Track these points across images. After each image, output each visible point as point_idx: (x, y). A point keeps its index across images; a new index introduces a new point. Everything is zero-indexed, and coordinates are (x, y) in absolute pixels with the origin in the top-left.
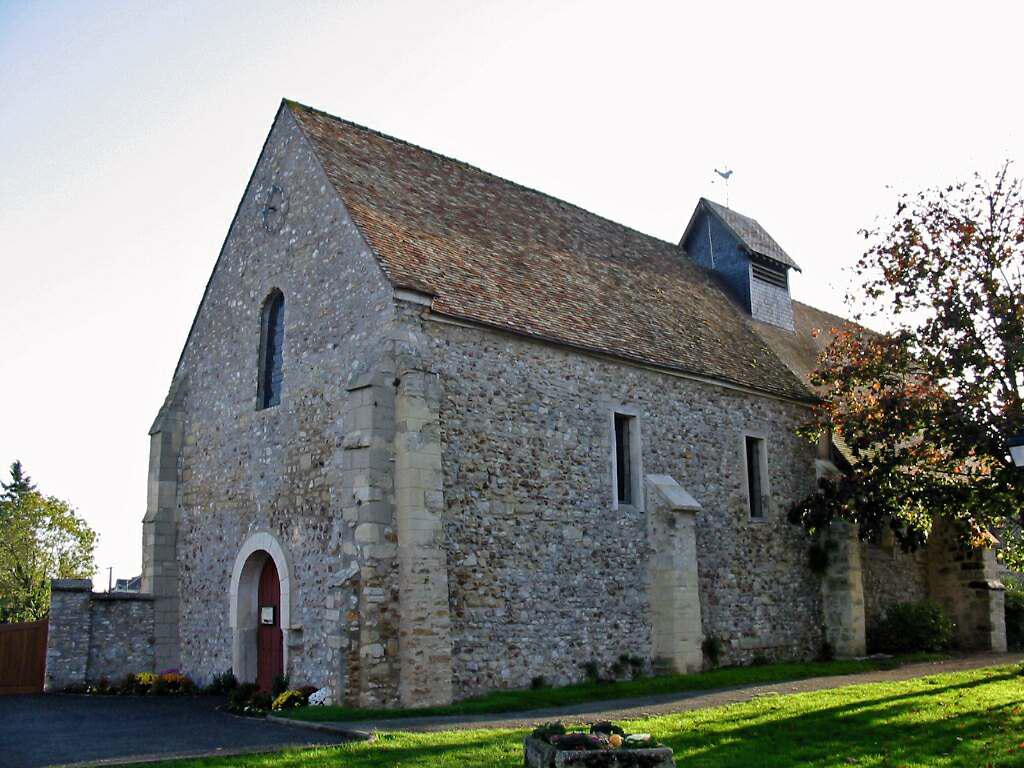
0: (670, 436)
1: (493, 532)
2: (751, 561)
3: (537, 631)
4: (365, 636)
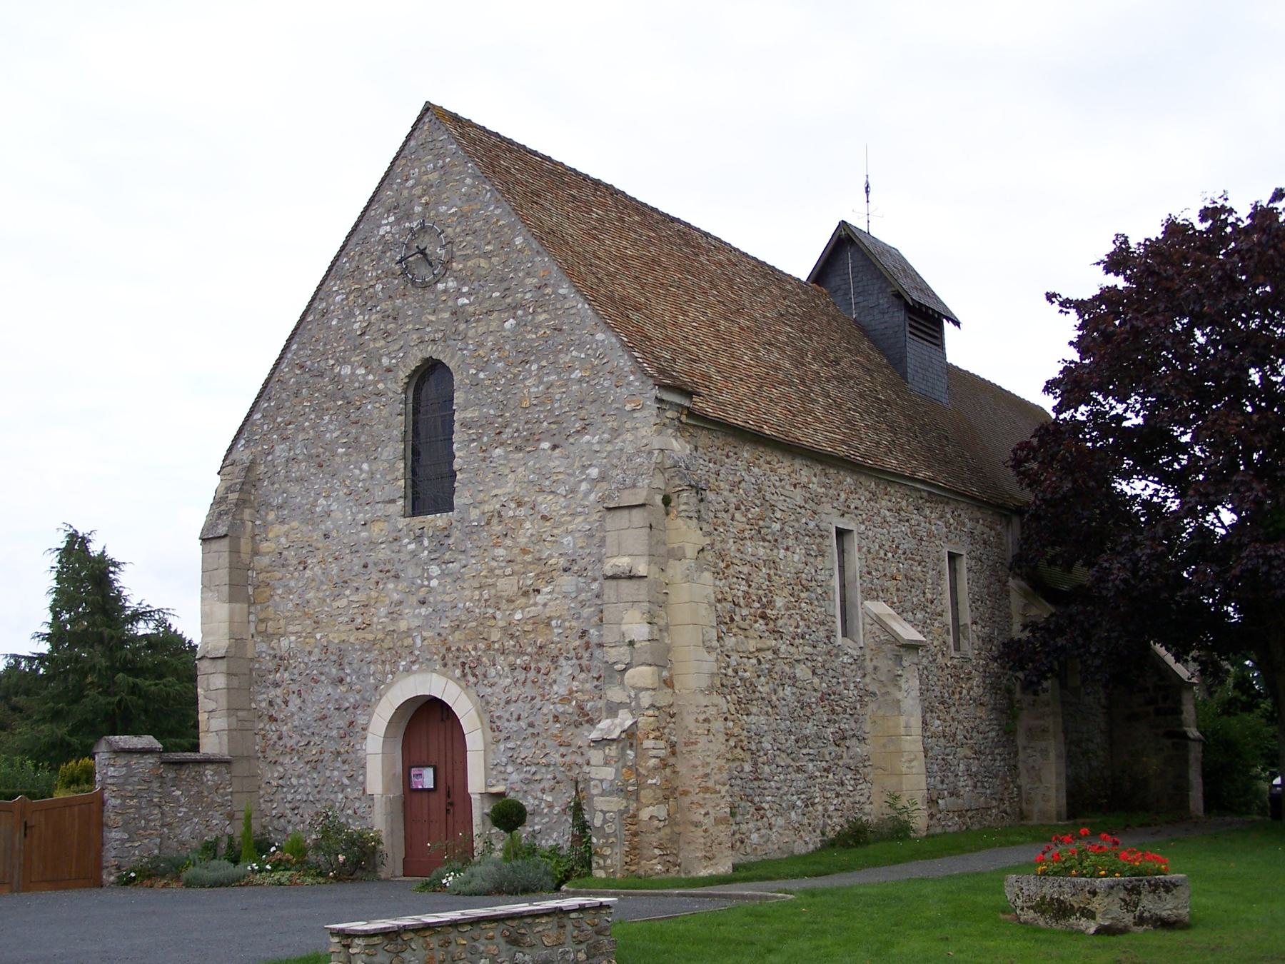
0: (882, 553)
1: (740, 673)
2: (954, 705)
3: (778, 789)
4: (646, 795)
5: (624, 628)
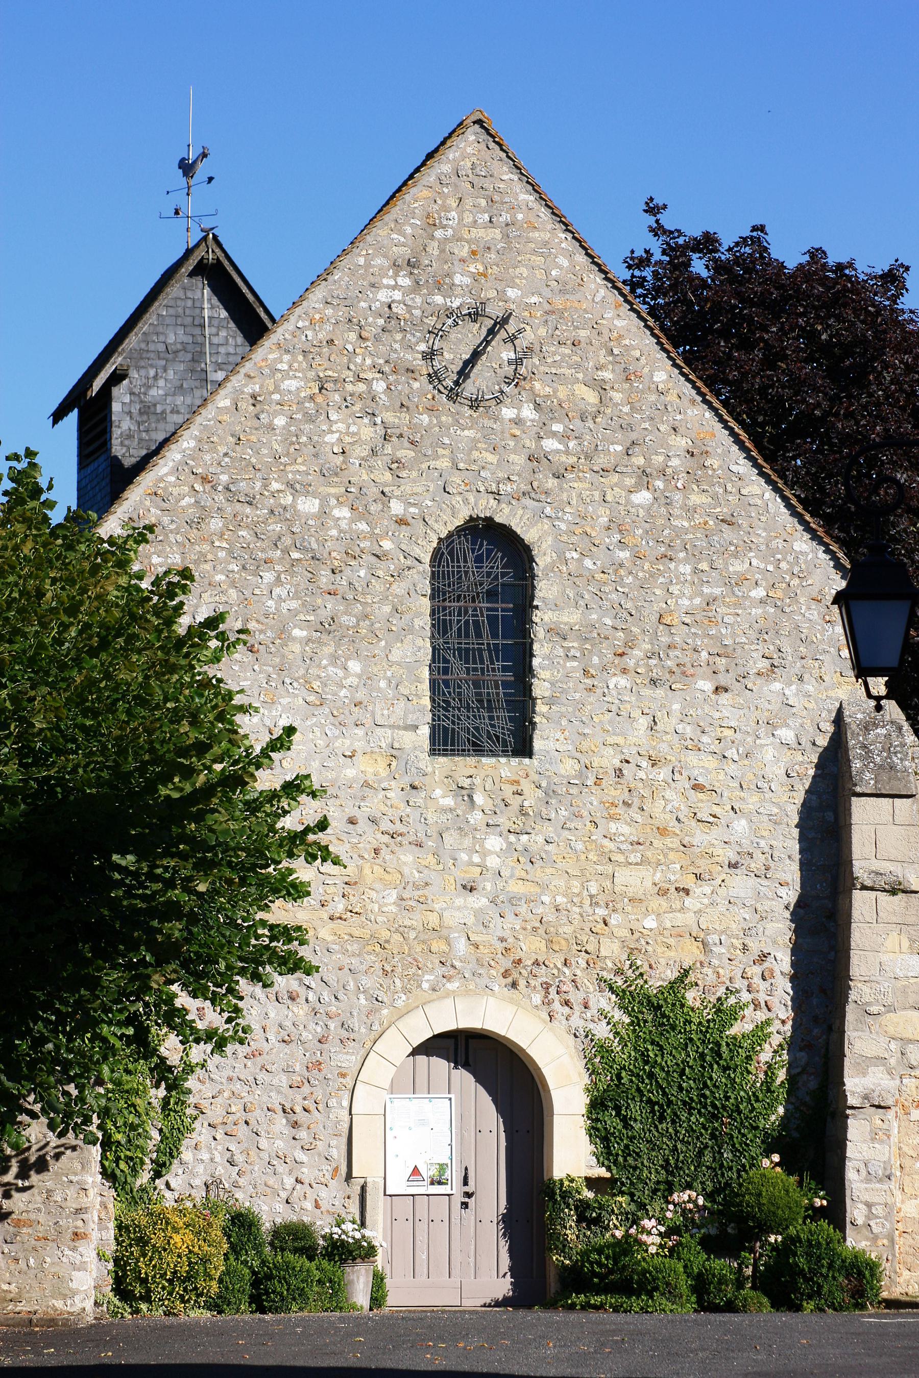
5: (884, 958)
